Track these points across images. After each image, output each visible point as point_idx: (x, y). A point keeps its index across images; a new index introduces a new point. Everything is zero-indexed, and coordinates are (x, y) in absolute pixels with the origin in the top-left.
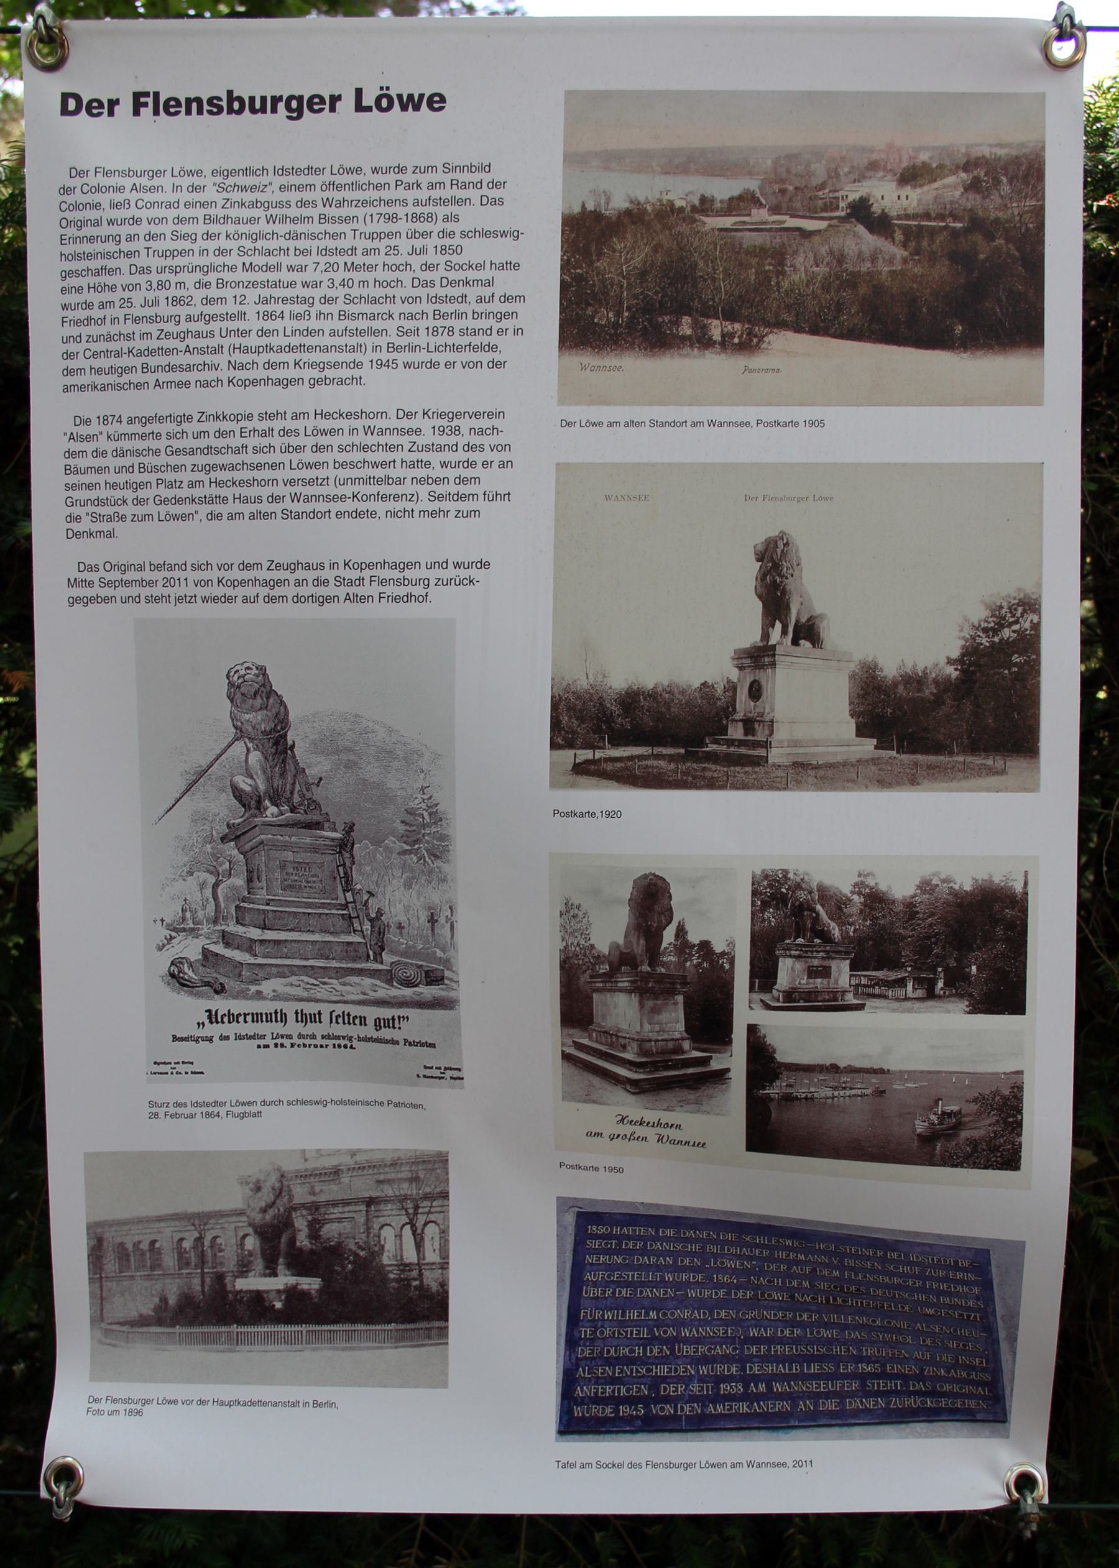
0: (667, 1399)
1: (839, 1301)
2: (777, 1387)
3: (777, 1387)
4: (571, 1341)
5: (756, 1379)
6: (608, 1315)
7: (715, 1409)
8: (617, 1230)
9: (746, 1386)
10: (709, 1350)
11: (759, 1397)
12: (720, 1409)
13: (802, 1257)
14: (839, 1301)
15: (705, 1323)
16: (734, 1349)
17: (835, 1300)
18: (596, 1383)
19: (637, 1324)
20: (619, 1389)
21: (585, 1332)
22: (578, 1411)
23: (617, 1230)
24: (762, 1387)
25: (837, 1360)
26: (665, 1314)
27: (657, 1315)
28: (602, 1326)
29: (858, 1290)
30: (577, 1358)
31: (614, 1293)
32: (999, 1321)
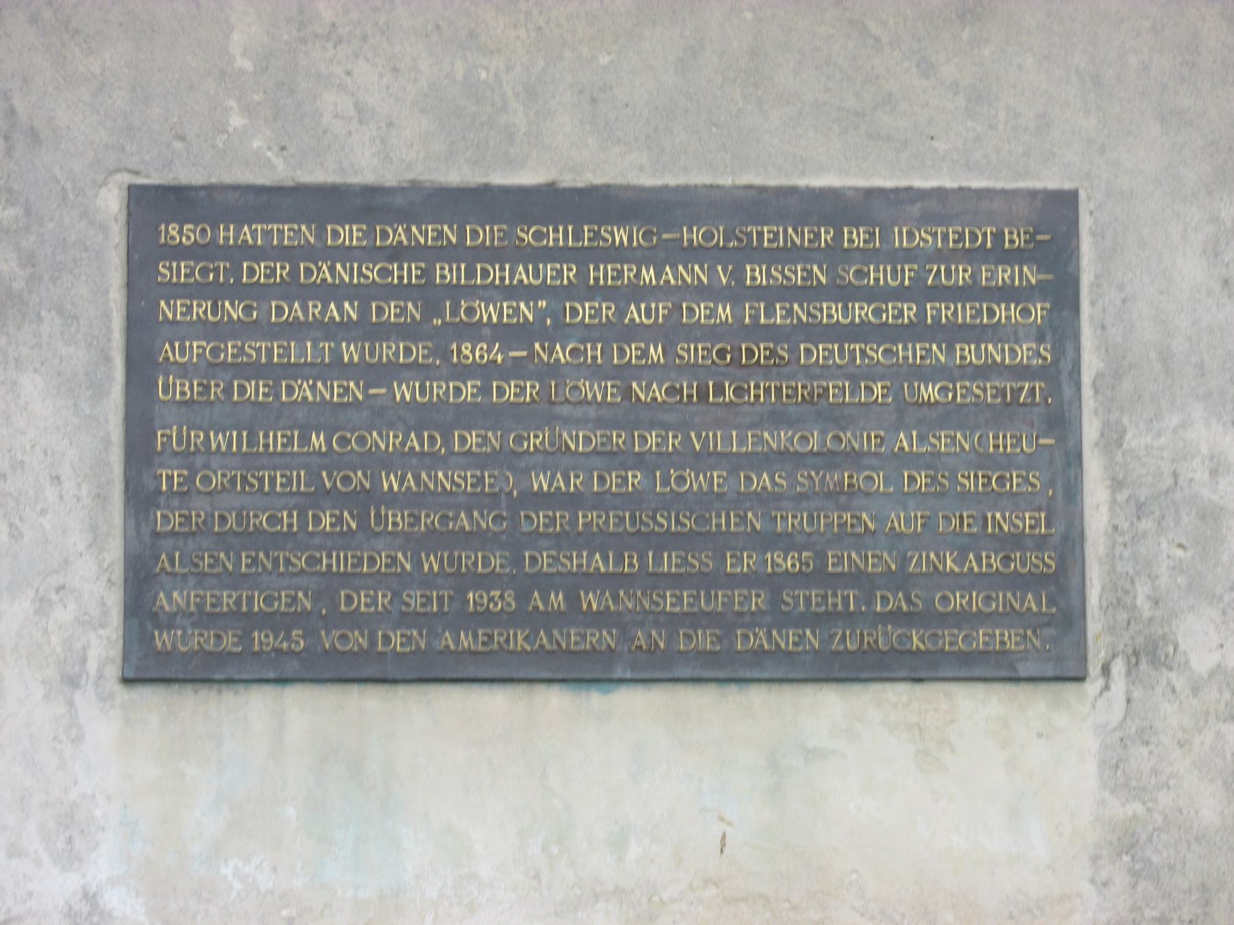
0: (354, 619)
1: (729, 394)
2: (591, 601)
3: (591, 601)
4: (140, 499)
5: (545, 583)
6: (218, 440)
7: (457, 641)
8: (226, 234)
9: (523, 597)
10: (444, 519)
11: (551, 619)
12: (466, 641)
13: (648, 275)
14: (729, 394)
15: (432, 460)
16: (498, 519)
17: (719, 390)
18: (199, 584)
19: (282, 460)
20: (250, 599)
21: (170, 476)
22: (163, 640)
23: (226, 234)
24: (558, 600)
25: (719, 543)
26: (344, 441)
27: (329, 442)
28: (207, 466)
29: (773, 353)
30: (156, 535)
31: (228, 391)
32: (1087, 392)
